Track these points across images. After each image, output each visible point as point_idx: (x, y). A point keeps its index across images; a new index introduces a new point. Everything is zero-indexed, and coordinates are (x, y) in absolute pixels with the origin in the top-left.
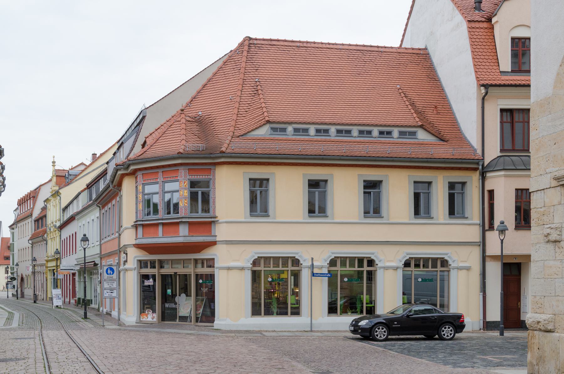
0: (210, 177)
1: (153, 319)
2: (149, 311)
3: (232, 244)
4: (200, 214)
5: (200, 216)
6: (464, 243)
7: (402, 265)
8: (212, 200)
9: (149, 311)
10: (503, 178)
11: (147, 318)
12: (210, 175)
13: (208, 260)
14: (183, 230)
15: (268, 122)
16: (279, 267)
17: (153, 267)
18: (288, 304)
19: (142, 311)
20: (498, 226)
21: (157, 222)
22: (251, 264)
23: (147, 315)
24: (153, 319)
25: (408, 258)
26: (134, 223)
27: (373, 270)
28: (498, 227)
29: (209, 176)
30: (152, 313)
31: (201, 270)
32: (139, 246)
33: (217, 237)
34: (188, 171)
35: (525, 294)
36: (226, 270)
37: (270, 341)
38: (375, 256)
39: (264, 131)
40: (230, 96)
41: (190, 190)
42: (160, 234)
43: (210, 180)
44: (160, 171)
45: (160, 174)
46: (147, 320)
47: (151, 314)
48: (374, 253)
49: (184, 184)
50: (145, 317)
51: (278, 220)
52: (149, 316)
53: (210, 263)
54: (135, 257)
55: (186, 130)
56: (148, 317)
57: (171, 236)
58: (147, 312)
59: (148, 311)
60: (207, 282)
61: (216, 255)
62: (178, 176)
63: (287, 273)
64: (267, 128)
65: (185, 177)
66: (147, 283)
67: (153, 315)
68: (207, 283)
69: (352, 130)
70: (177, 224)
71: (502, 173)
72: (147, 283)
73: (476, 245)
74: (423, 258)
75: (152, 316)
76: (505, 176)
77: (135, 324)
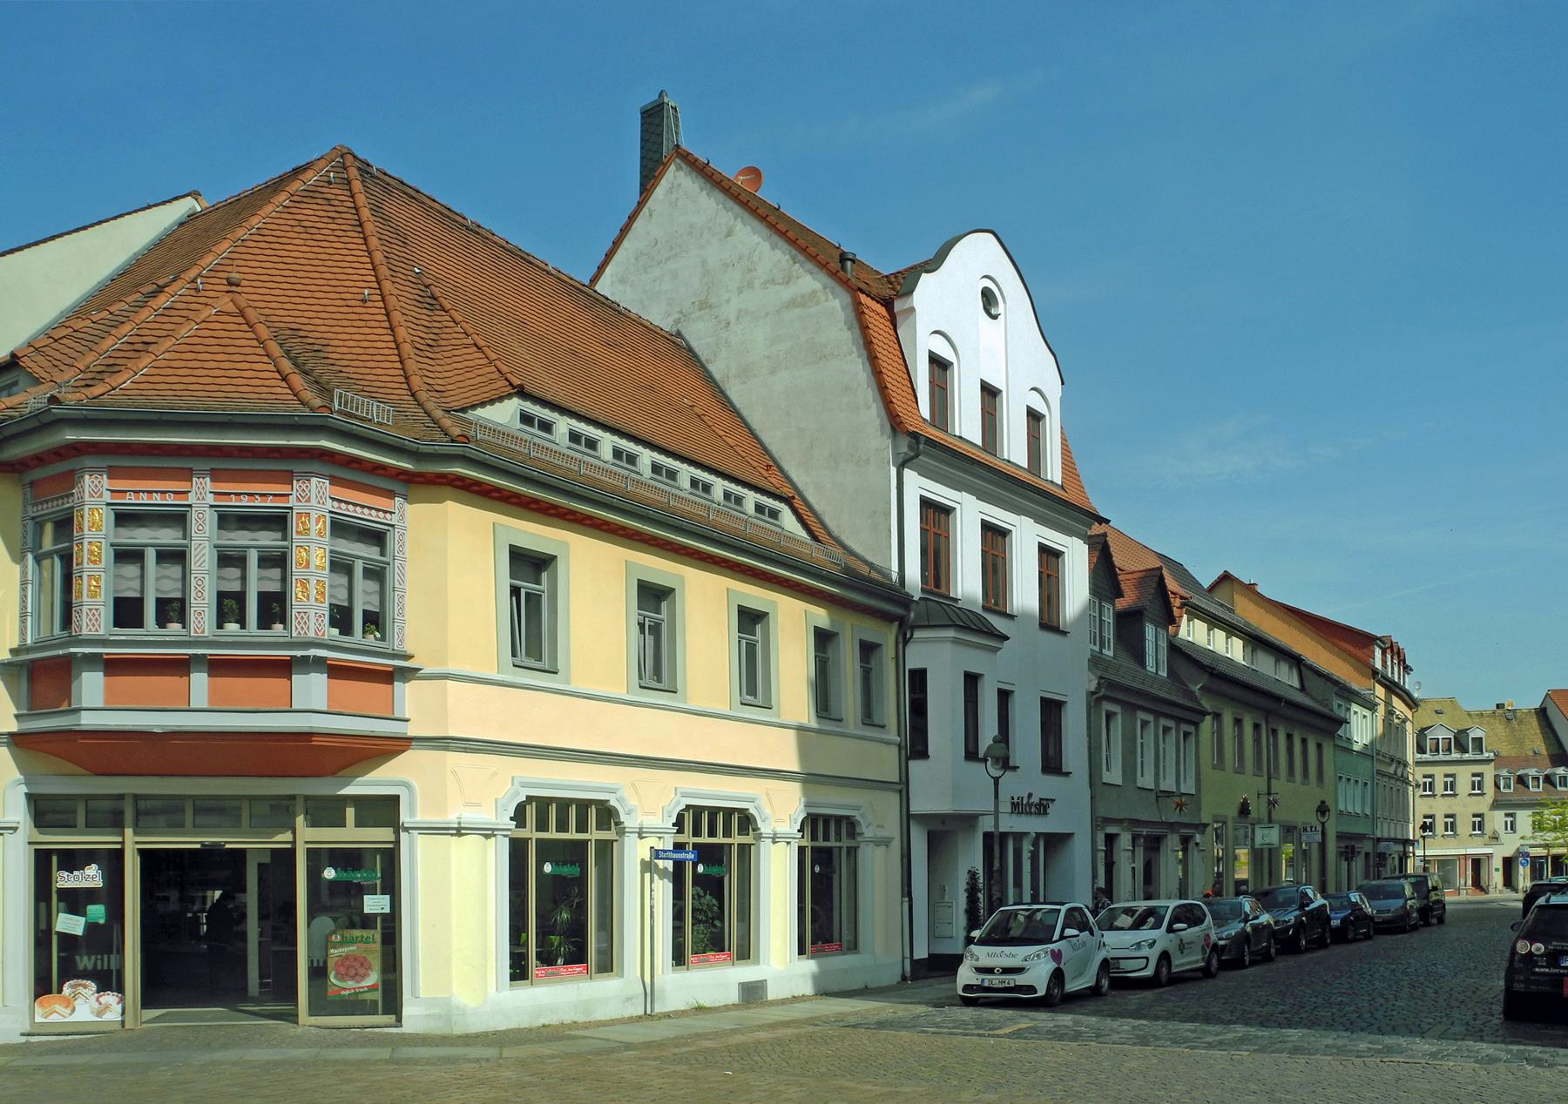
0: (391, 520)
1: (99, 1014)
2: (80, 985)
3: (465, 750)
5: (359, 647)
6: (822, 779)
8: (206, 594)
9: (80, 985)
10: (949, 645)
11: (69, 1011)
14: (312, 689)
15: (522, 393)
18: (673, 959)
20: (989, 748)
21: (190, 651)
22: (511, 819)
23: (69, 1003)
24: (99, 1014)
27: (836, 847)
28: (988, 748)
30: (98, 992)
31: (350, 834)
35: (946, 897)
39: (505, 413)
40: (366, 292)
41: (112, 545)
42: (200, 696)
43: (390, 528)
48: (755, 799)
49: (317, 525)
50: (58, 1008)
51: (573, 687)
52: (79, 1003)
53: (384, 810)
59: (72, 987)
62: (187, 492)
64: (514, 405)
65: (319, 502)
71: (951, 633)
73: (891, 790)
74: (823, 815)
75: (96, 1005)
76: (955, 641)
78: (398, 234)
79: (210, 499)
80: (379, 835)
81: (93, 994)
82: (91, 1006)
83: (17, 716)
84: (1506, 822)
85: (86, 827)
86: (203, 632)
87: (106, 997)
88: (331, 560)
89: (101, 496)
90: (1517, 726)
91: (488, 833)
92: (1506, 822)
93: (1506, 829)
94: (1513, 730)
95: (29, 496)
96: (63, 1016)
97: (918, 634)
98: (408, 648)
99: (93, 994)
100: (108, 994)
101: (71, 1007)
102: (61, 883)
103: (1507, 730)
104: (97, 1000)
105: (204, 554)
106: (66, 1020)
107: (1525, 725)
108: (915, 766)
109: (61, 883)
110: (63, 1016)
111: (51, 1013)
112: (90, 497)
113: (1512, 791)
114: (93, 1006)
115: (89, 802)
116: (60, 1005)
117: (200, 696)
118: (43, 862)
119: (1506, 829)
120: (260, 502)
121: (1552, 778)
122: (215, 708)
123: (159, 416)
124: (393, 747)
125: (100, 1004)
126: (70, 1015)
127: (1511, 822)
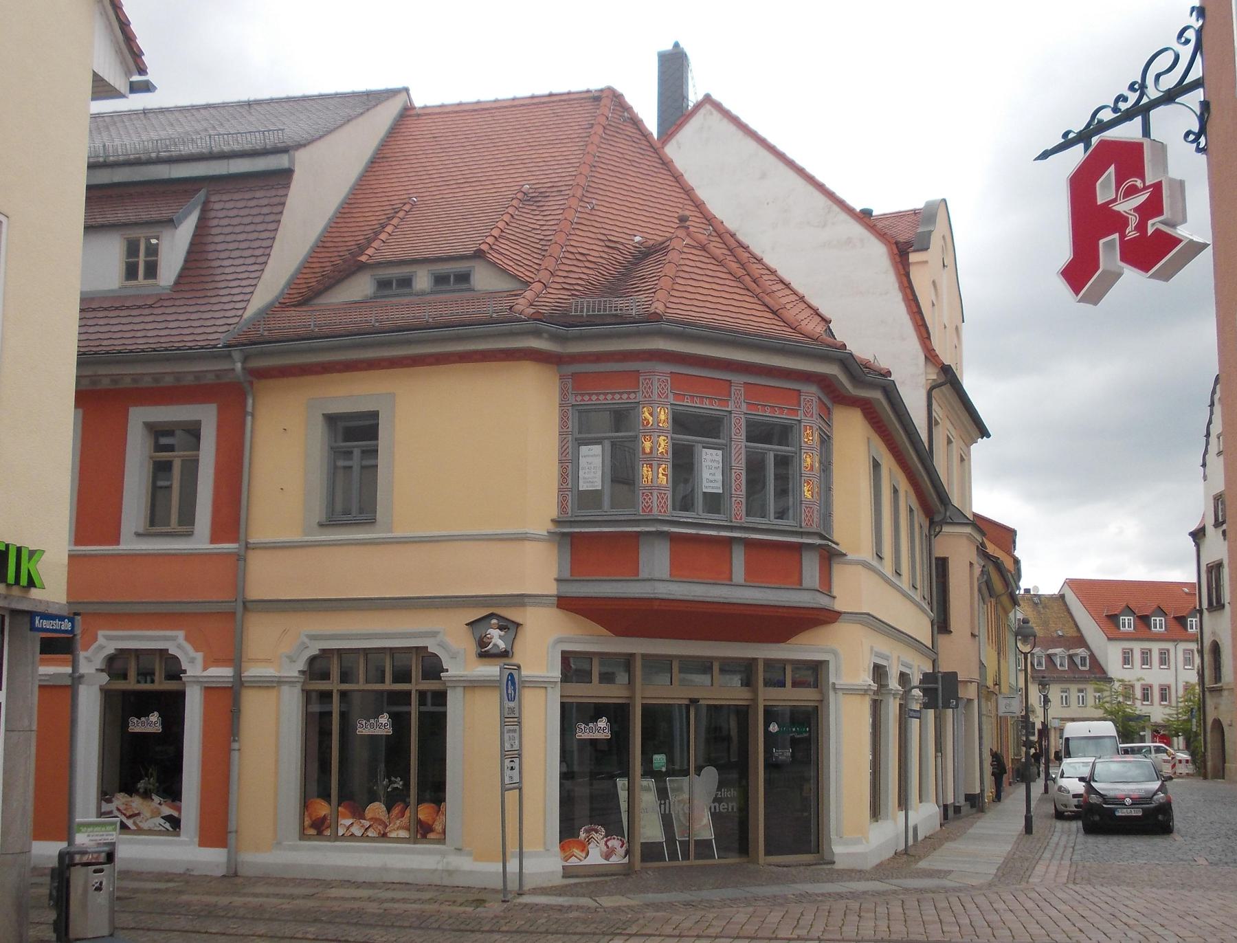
1: (607, 857)
4: (771, 521)
5: (768, 528)
7: (296, 674)
11: (584, 855)
12: (634, 392)
13: (799, 665)
16: (383, 681)
17: (607, 678)
19: (568, 831)
23: (584, 847)
24: (607, 857)
25: (314, 650)
26: (551, 527)
29: (632, 396)
32: (565, 603)
33: (836, 600)
34: (669, 379)
36: (859, 697)
37: (604, 925)
38: (441, 645)
42: (739, 572)
44: (738, 379)
45: (738, 391)
46: (585, 862)
47: (603, 842)
50: (576, 852)
51: (398, 534)
53: (814, 672)
54: (560, 641)
55: (502, 231)
56: (587, 854)
57: (776, 586)
58: (582, 835)
59: (587, 831)
60: (794, 729)
61: (835, 653)
63: (1096, 716)
66: (137, 726)
67: (610, 844)
68: (792, 732)
69: (470, 271)
70: (799, 548)
72: (137, 726)
77: (559, 881)
78: (643, 155)
79: (744, 407)
80: (805, 696)
81: (603, 838)
82: (600, 849)
83: (558, 580)
84: (1062, 697)
85: (591, 682)
86: (741, 519)
87: (613, 841)
88: (747, 451)
89: (667, 397)
90: (1042, 610)
91: (291, 683)
92: (1079, 696)
93: (1062, 703)
94: (1039, 612)
95: (570, 386)
96: (579, 859)
97: (946, 529)
98: (835, 538)
99: (603, 838)
100: (614, 838)
101: (586, 851)
102: (580, 734)
103: (1035, 613)
104: (606, 845)
105: (735, 449)
106: (581, 863)
107: (1049, 609)
108: (942, 640)
109: (580, 734)
110: (579, 859)
111: (570, 857)
112: (658, 397)
113: (1044, 668)
114: (603, 849)
115: (369, 656)
116: (577, 849)
117: (739, 572)
118: (566, 710)
119: (1062, 703)
120: (778, 414)
121: (1053, 658)
122: (748, 584)
123: (734, 337)
124: (824, 617)
125: (608, 847)
126: (585, 858)
127: (1066, 697)
